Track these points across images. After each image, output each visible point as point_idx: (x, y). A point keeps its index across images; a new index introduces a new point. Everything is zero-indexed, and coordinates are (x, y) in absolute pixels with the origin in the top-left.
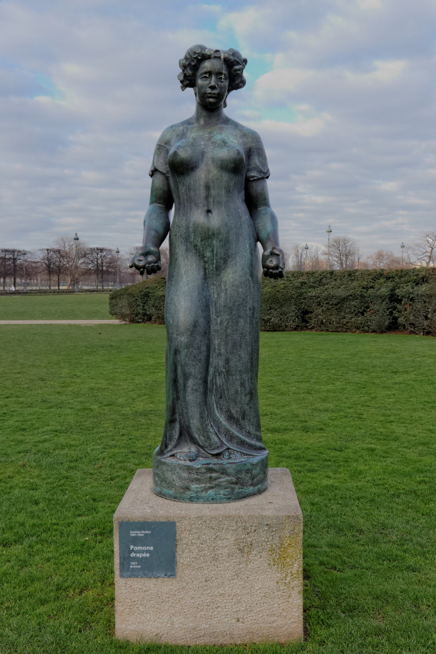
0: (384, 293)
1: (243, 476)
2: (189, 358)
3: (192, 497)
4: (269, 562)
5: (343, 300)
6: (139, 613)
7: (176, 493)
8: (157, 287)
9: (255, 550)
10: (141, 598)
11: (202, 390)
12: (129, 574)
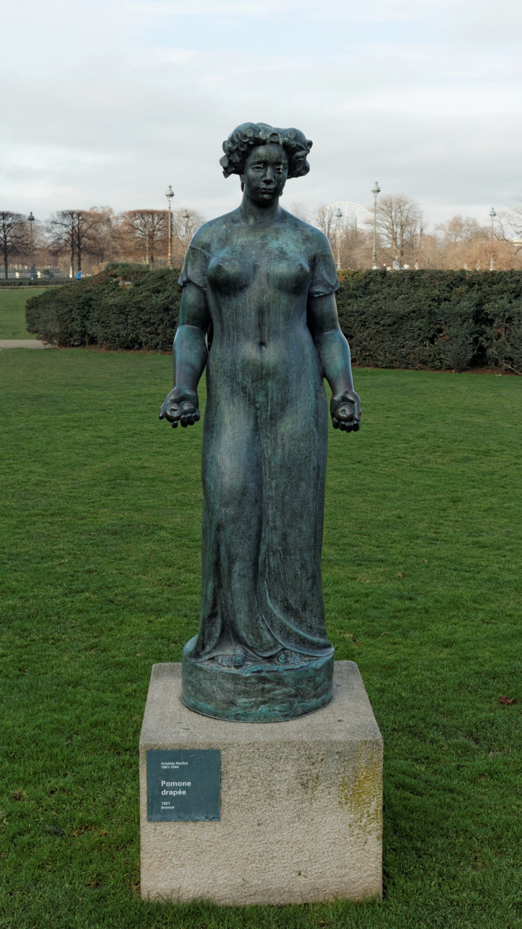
0: (465, 309)
1: (304, 686)
2: (236, 535)
3: (238, 714)
5: (401, 318)
6: (172, 867)
7: (216, 708)
8: (103, 290)
9: (322, 784)
12: (159, 817)
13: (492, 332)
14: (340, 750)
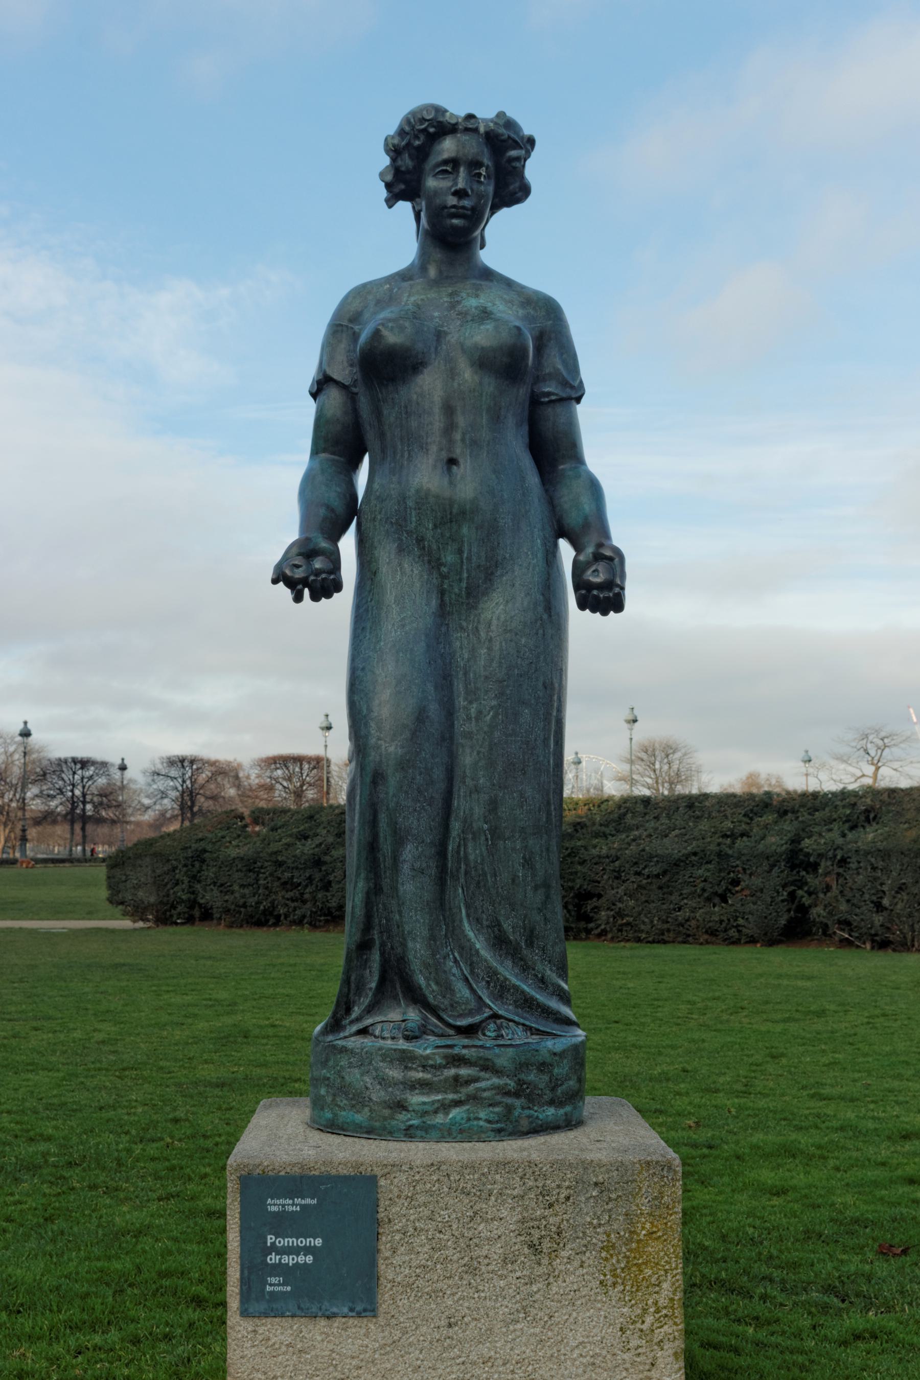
0: (774, 847)
2: (406, 792)
3: (411, 1126)
4: (602, 1277)
5: (675, 864)
7: (371, 1118)
8: (223, 837)
9: (569, 1246)
10: (291, 1368)
11: (433, 871)
12: (263, 1306)
13: (817, 882)
14: (600, 1179)
